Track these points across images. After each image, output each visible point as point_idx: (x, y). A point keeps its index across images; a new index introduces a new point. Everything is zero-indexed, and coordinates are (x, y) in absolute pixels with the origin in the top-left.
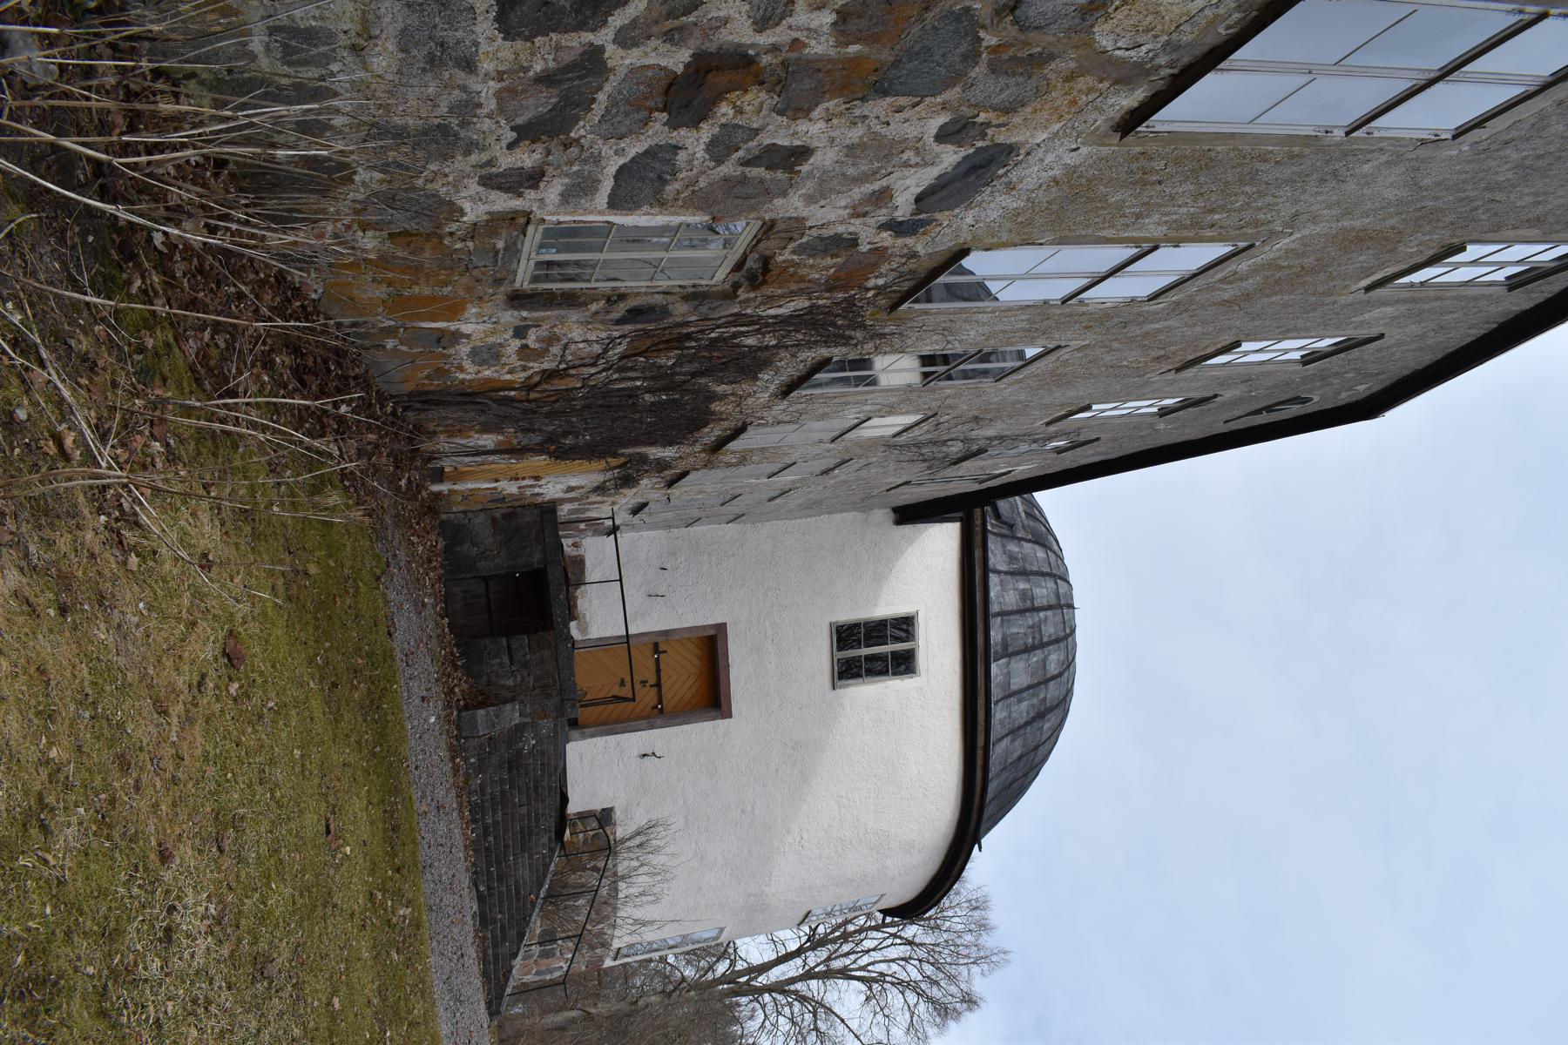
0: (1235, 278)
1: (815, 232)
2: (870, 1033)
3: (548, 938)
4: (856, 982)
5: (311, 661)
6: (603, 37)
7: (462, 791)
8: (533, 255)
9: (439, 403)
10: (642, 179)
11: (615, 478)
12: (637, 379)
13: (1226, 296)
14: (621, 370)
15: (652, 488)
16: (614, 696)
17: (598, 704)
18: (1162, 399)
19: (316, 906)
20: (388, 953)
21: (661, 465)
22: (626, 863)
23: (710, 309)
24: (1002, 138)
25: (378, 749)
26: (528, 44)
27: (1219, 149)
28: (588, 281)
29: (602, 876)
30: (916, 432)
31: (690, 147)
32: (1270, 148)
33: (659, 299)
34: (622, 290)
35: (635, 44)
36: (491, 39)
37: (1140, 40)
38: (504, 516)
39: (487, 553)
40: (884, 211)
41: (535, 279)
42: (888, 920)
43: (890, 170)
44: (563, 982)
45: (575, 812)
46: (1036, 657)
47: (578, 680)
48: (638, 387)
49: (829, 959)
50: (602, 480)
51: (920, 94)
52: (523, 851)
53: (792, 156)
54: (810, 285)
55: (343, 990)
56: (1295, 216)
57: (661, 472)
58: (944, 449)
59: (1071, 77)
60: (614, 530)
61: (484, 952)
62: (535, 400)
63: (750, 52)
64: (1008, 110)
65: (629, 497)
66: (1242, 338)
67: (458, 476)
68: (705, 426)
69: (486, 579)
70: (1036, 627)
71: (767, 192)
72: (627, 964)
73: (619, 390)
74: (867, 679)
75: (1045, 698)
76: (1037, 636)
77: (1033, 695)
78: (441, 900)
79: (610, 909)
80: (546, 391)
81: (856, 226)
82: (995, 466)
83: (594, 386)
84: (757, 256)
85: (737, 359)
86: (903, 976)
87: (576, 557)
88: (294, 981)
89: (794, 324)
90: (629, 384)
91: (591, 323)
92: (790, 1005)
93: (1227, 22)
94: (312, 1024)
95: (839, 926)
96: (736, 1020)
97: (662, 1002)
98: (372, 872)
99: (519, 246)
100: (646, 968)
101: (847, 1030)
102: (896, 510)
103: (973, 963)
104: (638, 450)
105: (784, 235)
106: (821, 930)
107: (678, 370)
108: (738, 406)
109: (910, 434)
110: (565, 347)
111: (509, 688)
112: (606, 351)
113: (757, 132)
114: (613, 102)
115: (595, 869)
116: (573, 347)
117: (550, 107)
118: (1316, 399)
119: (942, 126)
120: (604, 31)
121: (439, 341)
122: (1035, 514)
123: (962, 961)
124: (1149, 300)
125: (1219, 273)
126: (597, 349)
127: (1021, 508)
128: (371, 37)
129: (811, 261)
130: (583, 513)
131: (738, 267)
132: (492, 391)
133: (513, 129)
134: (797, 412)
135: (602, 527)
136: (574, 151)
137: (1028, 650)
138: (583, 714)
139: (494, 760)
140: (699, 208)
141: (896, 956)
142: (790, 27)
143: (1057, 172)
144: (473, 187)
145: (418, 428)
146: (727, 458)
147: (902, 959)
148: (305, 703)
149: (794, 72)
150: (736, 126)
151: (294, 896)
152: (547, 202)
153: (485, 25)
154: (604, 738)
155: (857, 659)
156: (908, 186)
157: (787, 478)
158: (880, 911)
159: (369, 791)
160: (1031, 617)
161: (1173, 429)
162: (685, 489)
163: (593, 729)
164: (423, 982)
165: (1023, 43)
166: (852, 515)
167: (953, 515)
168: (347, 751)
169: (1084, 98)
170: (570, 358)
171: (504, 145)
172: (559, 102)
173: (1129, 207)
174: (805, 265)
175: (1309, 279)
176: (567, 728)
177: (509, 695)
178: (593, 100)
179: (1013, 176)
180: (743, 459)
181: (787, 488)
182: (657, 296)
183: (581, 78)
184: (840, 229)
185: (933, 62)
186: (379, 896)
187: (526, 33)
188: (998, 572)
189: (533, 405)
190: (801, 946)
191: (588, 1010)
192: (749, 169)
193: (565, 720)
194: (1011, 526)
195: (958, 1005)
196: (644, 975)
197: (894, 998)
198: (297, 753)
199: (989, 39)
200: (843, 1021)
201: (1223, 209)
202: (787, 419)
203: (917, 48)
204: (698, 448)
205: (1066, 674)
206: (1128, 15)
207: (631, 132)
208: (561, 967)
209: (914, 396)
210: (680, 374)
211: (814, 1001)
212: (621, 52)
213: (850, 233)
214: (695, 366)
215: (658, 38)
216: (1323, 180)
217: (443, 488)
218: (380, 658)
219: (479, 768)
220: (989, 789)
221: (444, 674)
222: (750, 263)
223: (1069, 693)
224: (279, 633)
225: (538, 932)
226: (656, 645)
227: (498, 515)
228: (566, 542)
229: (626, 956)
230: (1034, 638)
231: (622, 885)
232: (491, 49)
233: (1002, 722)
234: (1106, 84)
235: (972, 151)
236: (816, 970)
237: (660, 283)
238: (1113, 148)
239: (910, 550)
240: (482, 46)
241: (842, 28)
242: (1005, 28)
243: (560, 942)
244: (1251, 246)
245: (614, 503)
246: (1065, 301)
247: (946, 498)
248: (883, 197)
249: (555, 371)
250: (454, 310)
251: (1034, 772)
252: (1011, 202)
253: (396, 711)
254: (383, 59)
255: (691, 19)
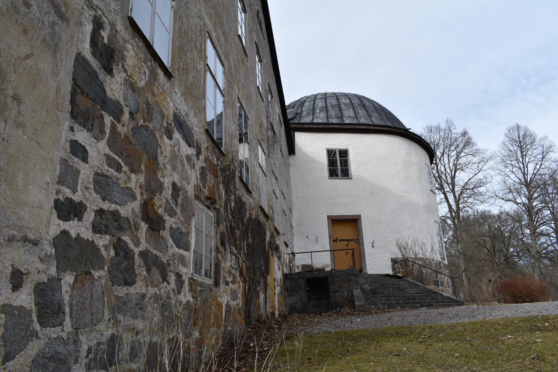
0: (218, 38)
1: (199, 182)
2: (475, 170)
3: (437, 283)
4: (456, 174)
5: (340, 358)
6: (136, 251)
7: (383, 311)
8: (202, 278)
9: (249, 313)
10: (180, 239)
11: (276, 253)
12: (243, 243)
13: (223, 40)
14: (240, 249)
15: (280, 240)
16: (352, 256)
17: (354, 262)
18: (256, 61)
19: (424, 360)
20: (440, 338)
21: (272, 236)
22: (411, 254)
23: (222, 218)
24: (171, 118)
25: (370, 338)
26: (138, 276)
27: (177, 44)
28: (211, 259)
29: (415, 263)
30: (264, 147)
31: (171, 223)
32: (177, 27)
33: (218, 235)
34: (215, 248)
35: (139, 240)
36: (136, 288)
37: (143, 71)
38: (287, 292)
39: (300, 299)
40: (193, 158)
41: (210, 277)
42: (434, 162)
43: (180, 156)
44: (452, 278)
45: (392, 272)
46: (343, 107)
47: (346, 269)
48: (246, 243)
49: (447, 183)
50: (276, 257)
51: (157, 145)
52: (405, 291)
53: (175, 189)
54: (216, 183)
55: (452, 352)
56: (199, 17)
57: (274, 237)
58: (270, 137)
59: (154, 95)
60: (293, 254)
61: (441, 306)
62: (249, 279)
63: (142, 202)
64: (163, 116)
65: (282, 248)
66: (237, 34)
67: (273, 307)
68: (260, 221)
69: (309, 299)
70: (333, 106)
71: (186, 197)
72: (446, 255)
73: (247, 250)
74: (349, 167)
75: (358, 104)
76: (336, 106)
77: (357, 108)
78: (422, 319)
79: (427, 261)
80: (246, 275)
81: (197, 167)
82: (276, 119)
83: (245, 259)
84: (206, 201)
85: (238, 209)
86: (455, 157)
87: (302, 268)
88: (449, 368)
89: (228, 189)
90: (245, 247)
91: (225, 259)
92: (464, 198)
93: (138, 42)
94: (463, 363)
95: (436, 179)
96: (468, 217)
97: (461, 243)
98: (412, 342)
99: (200, 282)
100: (448, 249)
101: (473, 178)
102: (290, 154)
103: (451, 132)
104: (267, 244)
105: (199, 192)
106: (437, 186)
107: (241, 229)
108: (254, 209)
109: (265, 149)
110: (232, 268)
111: (348, 293)
112: (234, 254)
113: (167, 201)
114: (156, 248)
115: (412, 265)
116: (232, 265)
117: (157, 270)
118: (258, 8)
119: (167, 138)
120: (135, 251)
121: (229, 311)
122: (293, 105)
123: (450, 136)
124: (224, 67)
125: (216, 43)
126: (233, 257)
127: (291, 110)
128: (134, 328)
129: (208, 183)
130: (287, 264)
131: (209, 208)
132: (246, 294)
133: (163, 283)
134: (256, 189)
135: (292, 258)
136: (171, 262)
137: (340, 110)
138: (358, 267)
139: (373, 299)
140: (190, 221)
141: (447, 159)
142: (135, 189)
143: (183, 99)
144: (181, 297)
145: (257, 321)
146: (271, 213)
147: (448, 157)
148: (355, 361)
149: (149, 188)
150: (165, 208)
151: (420, 367)
152: (187, 272)
153: (132, 290)
154: (366, 260)
155: (342, 170)
156: (186, 150)
157: (278, 192)
158: (431, 165)
159: (384, 342)
160: (329, 108)
161: (266, 57)
162: (280, 228)
163: (363, 264)
164: (450, 326)
165: (143, 111)
166: (291, 170)
167: (292, 134)
168: (371, 348)
169: (160, 90)
170: (236, 266)
171: (168, 286)
172: (156, 267)
173: (194, 74)
174: (209, 185)
175: (219, 12)
176: (362, 273)
177: (350, 293)
178: (155, 255)
179: (184, 114)
180: (271, 208)
181: (281, 192)
182: (217, 236)
183: (148, 259)
184: (198, 173)
185: (147, 141)
186: (420, 340)
187: (134, 276)
188: (313, 119)
189: (251, 280)
190: (442, 193)
191: (462, 270)
192: (179, 203)
193: (360, 274)
194: (297, 114)
195: (466, 138)
196: (451, 249)
197: (462, 160)
198: (372, 364)
199: (141, 122)
200: (470, 179)
201: (196, 42)
202: (258, 192)
203: (143, 146)
204: (267, 223)
205: (350, 96)
206: (135, 76)
207: (166, 243)
208: (447, 279)
209: (252, 148)
210: (242, 229)
211: (462, 189)
212: (141, 245)
213: (200, 169)
214: (240, 224)
215: (137, 233)
216: (188, 8)
217: (277, 313)
218: (338, 336)
219: (376, 304)
220: (389, 125)
221: (342, 316)
222: (208, 204)
223: (356, 96)
224: (331, 368)
225: (434, 287)
226: (334, 241)
227: (287, 294)
228: (297, 271)
229: (444, 256)
230: (336, 108)
231: (419, 256)
232: (139, 288)
233: (366, 120)
234: (156, 83)
235: (175, 128)
236: (451, 188)
237: (213, 235)
238: (176, 80)
239: (304, 150)
240: (138, 291)
241: (136, 171)
242: (138, 117)
243: (438, 279)
244: (208, 32)
245: (284, 253)
246: (223, 96)
247: (286, 136)
248: (188, 158)
249: (240, 272)
250: (219, 305)
251: (384, 109)
252: (192, 114)
253: (356, 332)
254: (140, 324)
255: (132, 221)
